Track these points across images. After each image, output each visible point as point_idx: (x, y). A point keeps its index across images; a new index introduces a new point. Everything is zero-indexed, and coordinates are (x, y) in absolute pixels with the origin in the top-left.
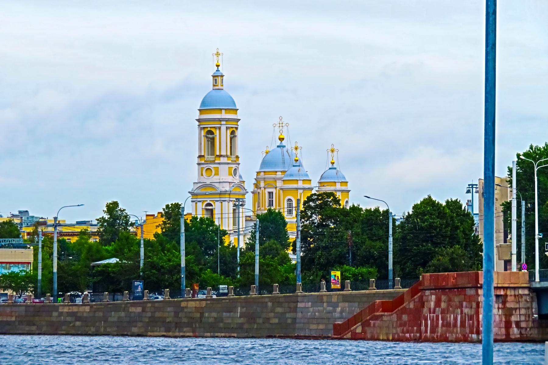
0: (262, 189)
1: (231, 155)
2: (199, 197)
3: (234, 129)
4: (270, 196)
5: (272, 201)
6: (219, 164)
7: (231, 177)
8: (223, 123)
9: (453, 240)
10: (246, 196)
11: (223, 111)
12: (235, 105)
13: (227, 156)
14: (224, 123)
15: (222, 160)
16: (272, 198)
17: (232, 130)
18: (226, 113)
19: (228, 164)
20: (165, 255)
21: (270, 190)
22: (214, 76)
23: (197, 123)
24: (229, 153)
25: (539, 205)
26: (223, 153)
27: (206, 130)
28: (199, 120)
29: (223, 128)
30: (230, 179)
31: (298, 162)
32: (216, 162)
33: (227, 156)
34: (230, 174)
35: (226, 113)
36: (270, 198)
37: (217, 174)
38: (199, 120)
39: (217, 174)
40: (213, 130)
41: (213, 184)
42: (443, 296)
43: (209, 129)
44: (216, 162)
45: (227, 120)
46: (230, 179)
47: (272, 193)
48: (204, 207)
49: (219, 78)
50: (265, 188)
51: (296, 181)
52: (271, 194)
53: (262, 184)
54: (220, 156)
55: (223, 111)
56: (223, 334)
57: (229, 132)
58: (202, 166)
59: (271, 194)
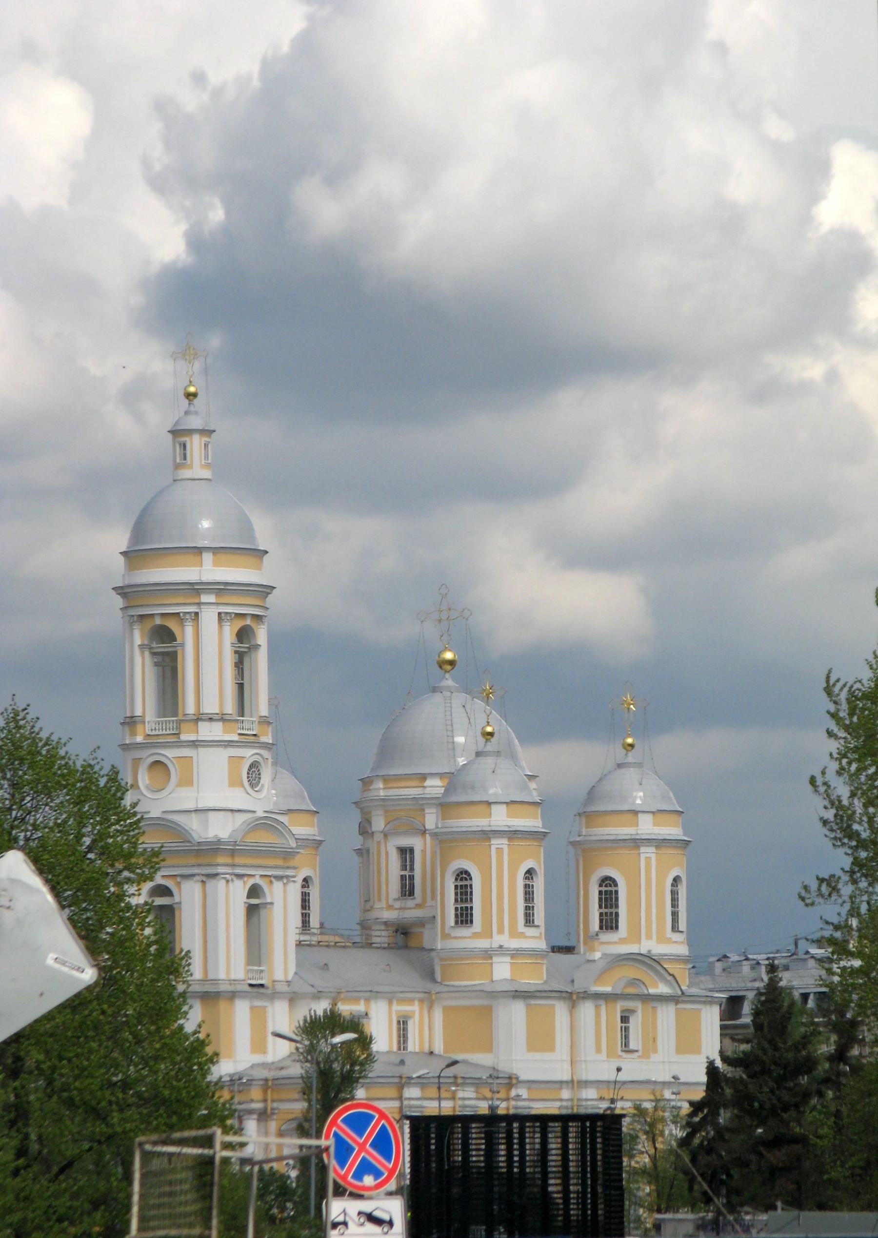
0: (378, 837)
1: (241, 712)
2: (238, 860)
4: (404, 861)
5: (412, 878)
6: (195, 744)
7: (238, 792)
8: (205, 598)
11: (207, 557)
12: (252, 537)
13: (223, 718)
14: (212, 598)
16: (412, 869)
17: (239, 624)
18: (216, 564)
19: (228, 744)
21: (406, 841)
22: (176, 433)
23: (119, 602)
24: (230, 708)
25: (125, 663)
26: (210, 706)
27: (149, 624)
28: (123, 591)
29: (209, 617)
30: (237, 798)
31: (494, 740)
32: (184, 737)
33: (223, 718)
34: (234, 782)
36: (404, 867)
37: (187, 781)
38: (123, 591)
39: (187, 781)
40: (172, 625)
43: (158, 621)
44: (184, 737)
45: (222, 589)
46: (237, 798)
47: (412, 850)
49: (196, 438)
50: (386, 836)
51: (630, 816)
52: (406, 853)
53: (379, 823)
54: (199, 718)
55: (207, 557)
56: (589, 1103)
57: (229, 632)
58: (138, 754)
59: (406, 853)
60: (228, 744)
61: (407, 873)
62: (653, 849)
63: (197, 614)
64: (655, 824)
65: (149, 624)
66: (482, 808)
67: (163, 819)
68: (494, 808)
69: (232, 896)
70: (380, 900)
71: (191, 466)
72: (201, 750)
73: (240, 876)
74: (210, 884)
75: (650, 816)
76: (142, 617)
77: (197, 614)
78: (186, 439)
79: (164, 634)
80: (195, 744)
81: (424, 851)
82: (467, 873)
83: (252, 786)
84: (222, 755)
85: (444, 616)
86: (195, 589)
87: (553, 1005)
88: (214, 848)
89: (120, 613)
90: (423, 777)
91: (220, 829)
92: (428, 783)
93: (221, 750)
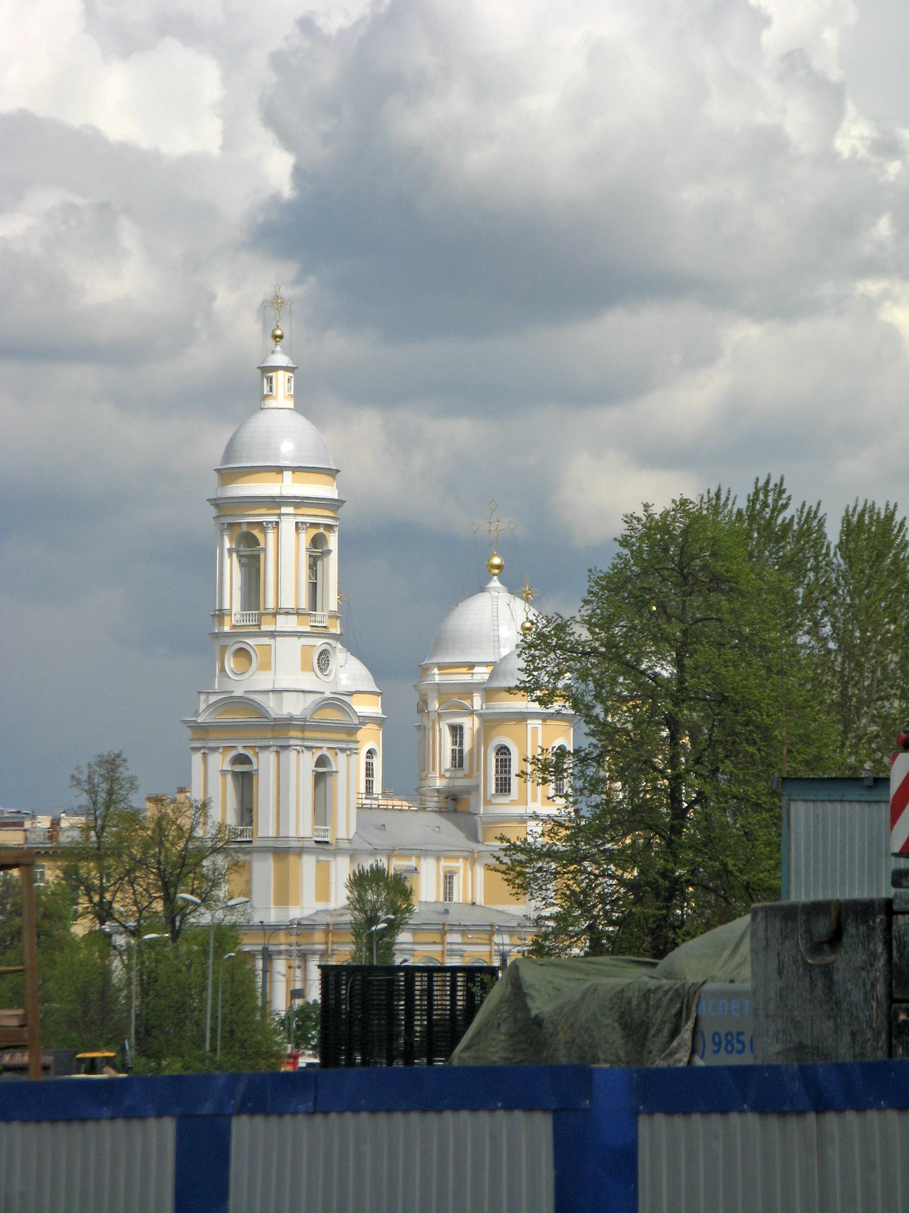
3: (321, 530)
6: (273, 634)
7: (310, 676)
8: (284, 510)
9: (188, 905)
10: (360, 733)
11: (288, 475)
13: (298, 613)
14: (291, 510)
15: (285, 623)
17: (313, 532)
18: (294, 481)
20: (547, 890)
21: (456, 721)
23: (213, 511)
24: (304, 604)
26: (287, 602)
29: (288, 525)
30: (308, 681)
32: (264, 628)
33: (298, 613)
34: (306, 666)
35: (294, 481)
37: (266, 666)
39: (266, 666)
41: (258, 698)
42: (688, 738)
43: (245, 529)
45: (299, 502)
46: (308, 681)
47: (461, 728)
48: (228, 767)
52: (457, 731)
57: (305, 538)
63: (277, 523)
73: (309, 748)
76: (231, 525)
77: (277, 523)
80: (273, 634)
84: (297, 643)
86: (276, 502)
90: (471, 666)
91: (293, 707)
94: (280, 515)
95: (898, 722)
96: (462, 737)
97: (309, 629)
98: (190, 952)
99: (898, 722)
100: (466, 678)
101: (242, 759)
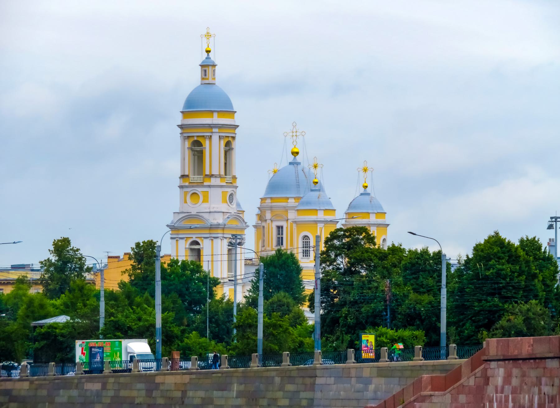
1: (226, 175)
2: (181, 232)
3: (230, 139)
4: (279, 231)
6: (209, 186)
8: (214, 130)
11: (215, 114)
13: (220, 176)
16: (282, 234)
17: (227, 140)
18: (218, 117)
19: (222, 186)
21: (280, 224)
23: (179, 131)
24: (223, 173)
26: (215, 172)
28: (181, 127)
29: (215, 138)
30: (224, 207)
32: (205, 184)
33: (220, 176)
34: (224, 201)
36: (279, 234)
37: (206, 200)
39: (206, 200)
40: (201, 140)
41: (201, 214)
43: (195, 139)
44: (205, 184)
46: (224, 207)
47: (282, 227)
49: (210, 68)
50: (272, 221)
53: (268, 215)
54: (212, 176)
55: (215, 114)
57: (223, 143)
59: (280, 228)
60: (222, 186)
61: (280, 236)
62: (376, 228)
63: (211, 136)
64: (377, 218)
65: (192, 140)
66: (333, 212)
67: (198, 215)
68: (371, 215)
69: (222, 246)
70: (269, 246)
71: (208, 79)
72: (212, 189)
73: (225, 238)
74: (215, 240)
75: (375, 215)
76: (189, 137)
77: (211, 136)
78: (207, 68)
79: (197, 143)
80: (209, 186)
81: (287, 228)
82: (307, 236)
83: (231, 203)
84: (220, 190)
85: (294, 134)
86: (211, 126)
87: (121, 342)
88: (216, 227)
89: (180, 135)
90: (288, 198)
91: (219, 219)
92: (289, 201)
93: (219, 189)
94: (212, 132)
95: (516, 274)
96: (282, 231)
97: (225, 184)
98: (375, 276)
99: (516, 274)
100: (284, 204)
101: (196, 243)
